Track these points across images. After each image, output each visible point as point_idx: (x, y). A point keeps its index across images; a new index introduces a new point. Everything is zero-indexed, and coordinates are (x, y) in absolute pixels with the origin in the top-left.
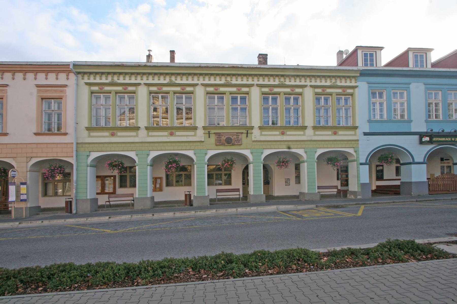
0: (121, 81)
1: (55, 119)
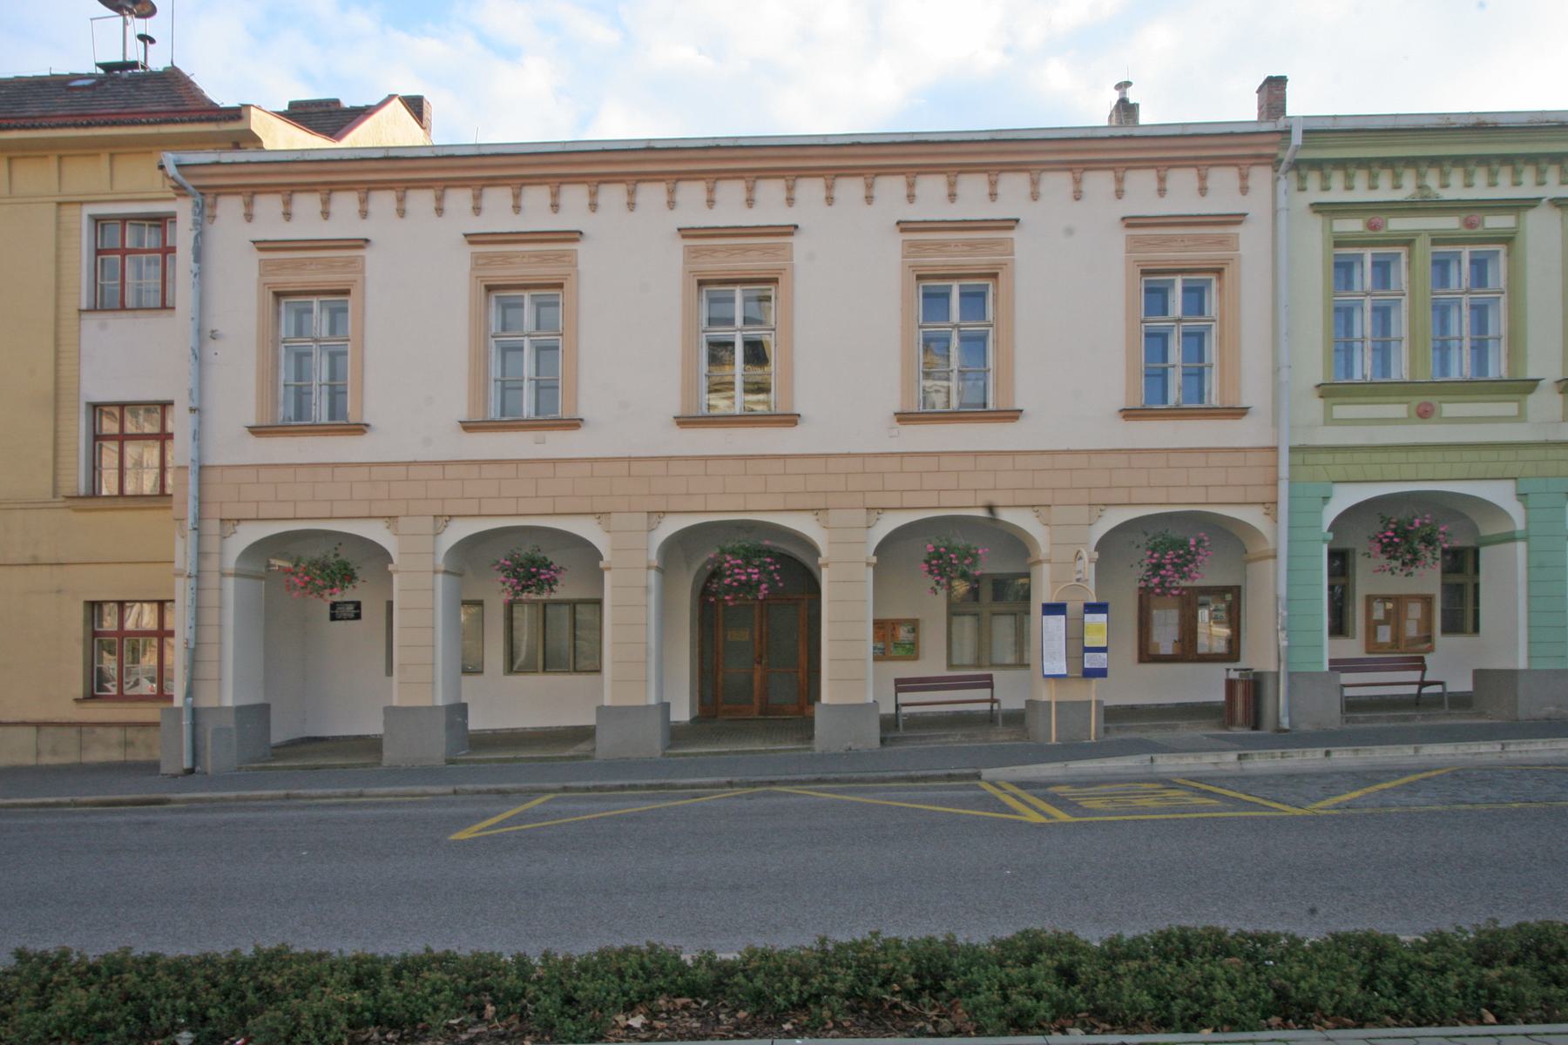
0: (1455, 191)
1: (320, 370)
